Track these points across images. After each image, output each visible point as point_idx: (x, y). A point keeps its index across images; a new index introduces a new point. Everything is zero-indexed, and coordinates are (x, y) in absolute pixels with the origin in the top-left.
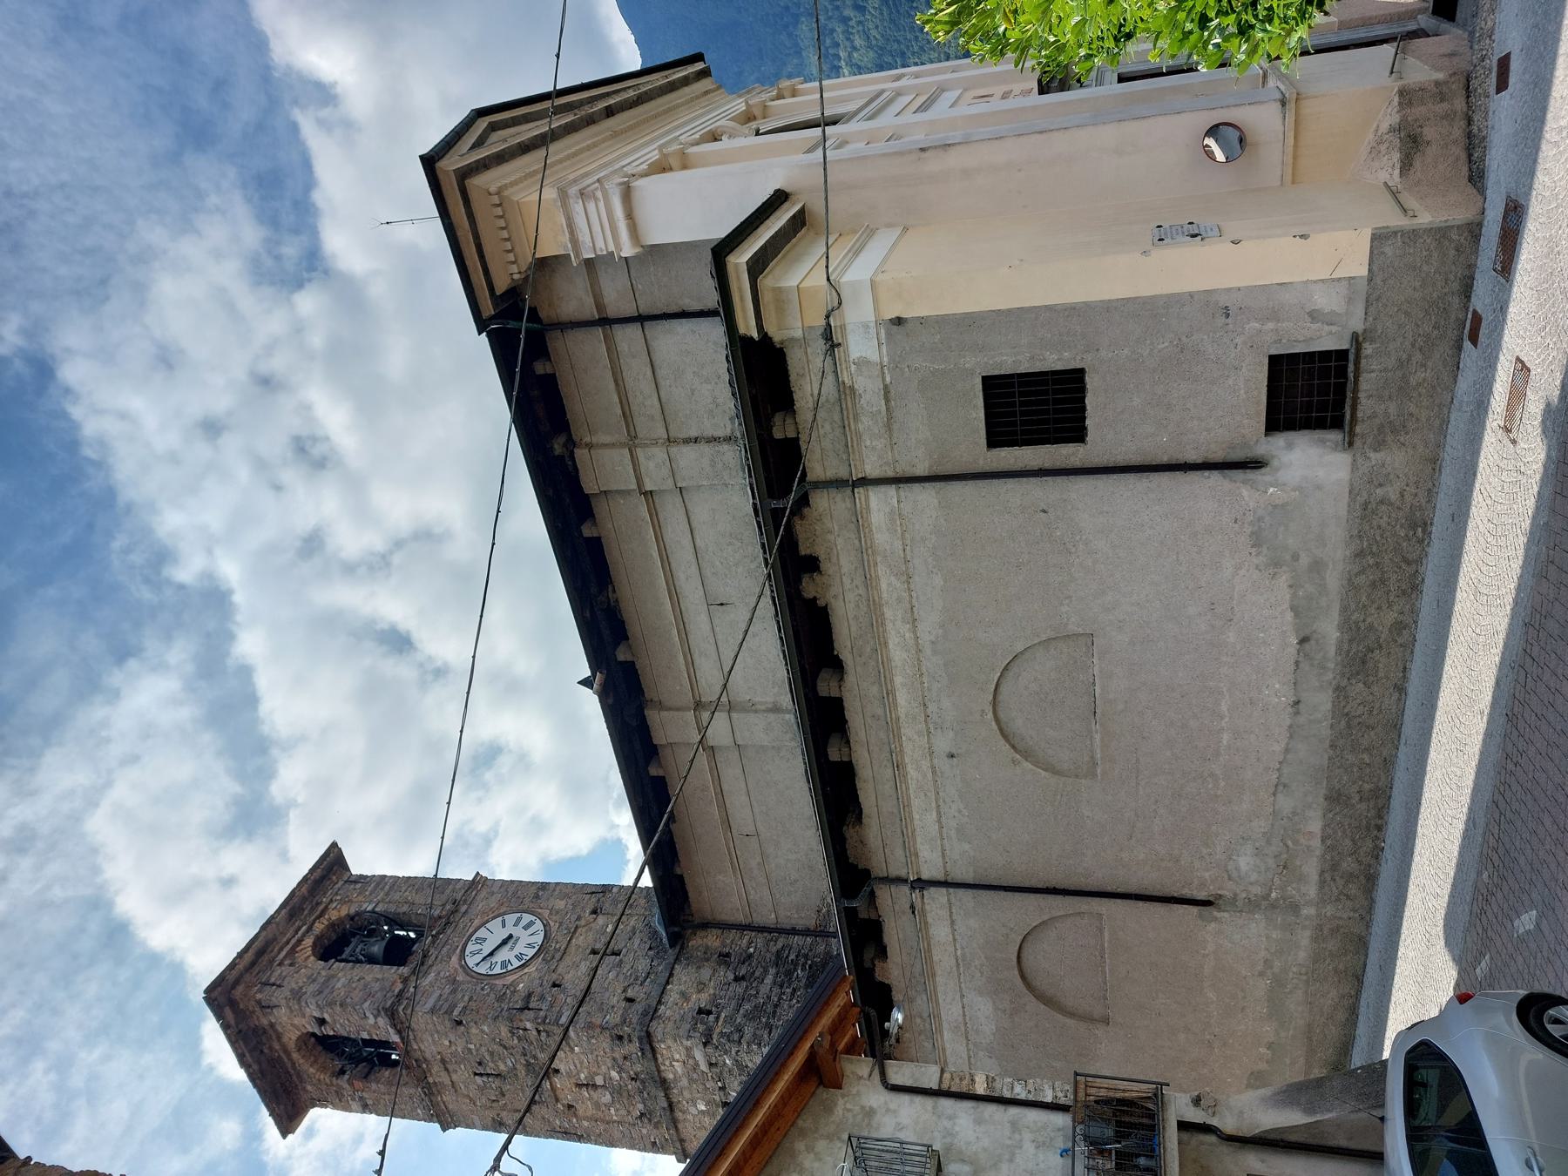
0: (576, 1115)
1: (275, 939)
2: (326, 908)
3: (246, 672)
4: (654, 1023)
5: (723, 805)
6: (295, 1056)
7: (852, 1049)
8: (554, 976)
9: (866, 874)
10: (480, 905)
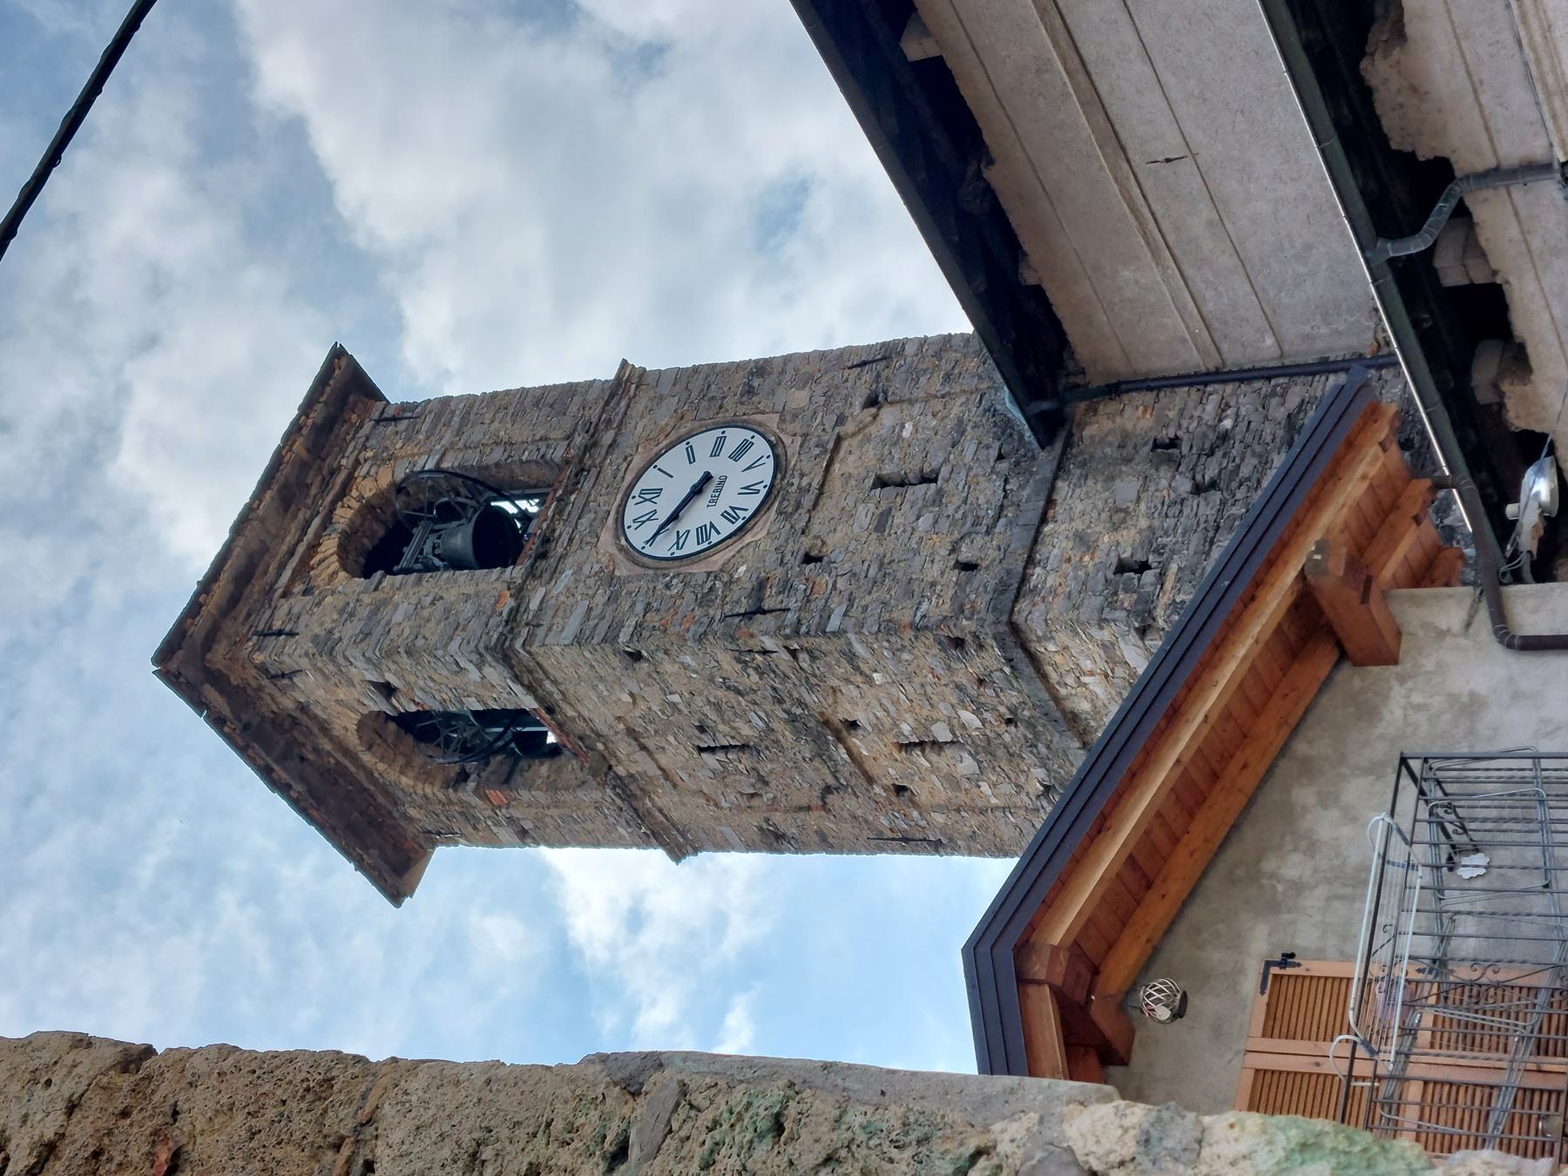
0: (915, 805)
1: (264, 550)
2: (351, 478)
3: (294, 131)
4: (1023, 605)
5: (1094, 101)
6: (367, 758)
7: (1428, 572)
8: (806, 543)
9: (1440, 172)
10: (639, 427)
